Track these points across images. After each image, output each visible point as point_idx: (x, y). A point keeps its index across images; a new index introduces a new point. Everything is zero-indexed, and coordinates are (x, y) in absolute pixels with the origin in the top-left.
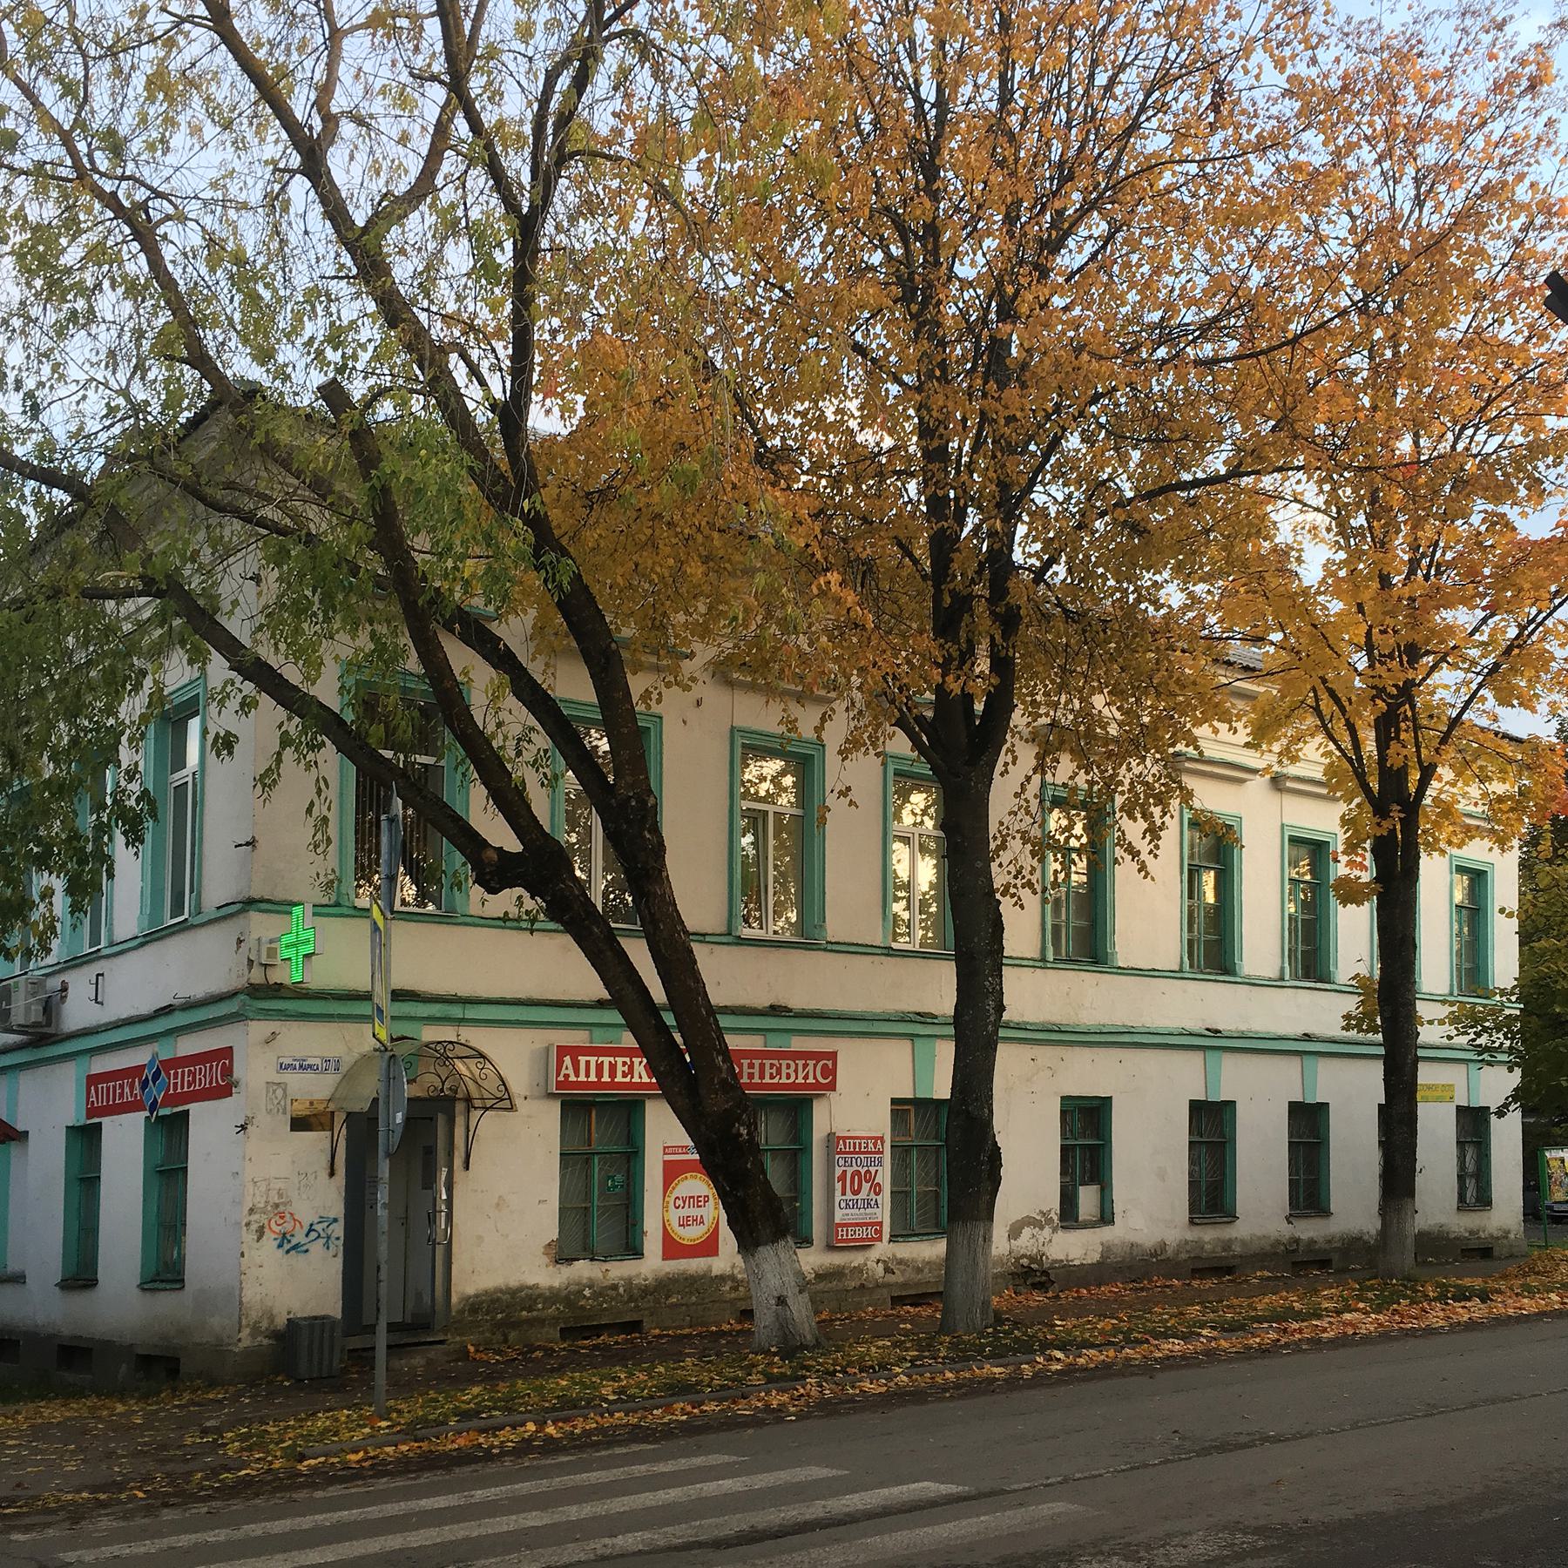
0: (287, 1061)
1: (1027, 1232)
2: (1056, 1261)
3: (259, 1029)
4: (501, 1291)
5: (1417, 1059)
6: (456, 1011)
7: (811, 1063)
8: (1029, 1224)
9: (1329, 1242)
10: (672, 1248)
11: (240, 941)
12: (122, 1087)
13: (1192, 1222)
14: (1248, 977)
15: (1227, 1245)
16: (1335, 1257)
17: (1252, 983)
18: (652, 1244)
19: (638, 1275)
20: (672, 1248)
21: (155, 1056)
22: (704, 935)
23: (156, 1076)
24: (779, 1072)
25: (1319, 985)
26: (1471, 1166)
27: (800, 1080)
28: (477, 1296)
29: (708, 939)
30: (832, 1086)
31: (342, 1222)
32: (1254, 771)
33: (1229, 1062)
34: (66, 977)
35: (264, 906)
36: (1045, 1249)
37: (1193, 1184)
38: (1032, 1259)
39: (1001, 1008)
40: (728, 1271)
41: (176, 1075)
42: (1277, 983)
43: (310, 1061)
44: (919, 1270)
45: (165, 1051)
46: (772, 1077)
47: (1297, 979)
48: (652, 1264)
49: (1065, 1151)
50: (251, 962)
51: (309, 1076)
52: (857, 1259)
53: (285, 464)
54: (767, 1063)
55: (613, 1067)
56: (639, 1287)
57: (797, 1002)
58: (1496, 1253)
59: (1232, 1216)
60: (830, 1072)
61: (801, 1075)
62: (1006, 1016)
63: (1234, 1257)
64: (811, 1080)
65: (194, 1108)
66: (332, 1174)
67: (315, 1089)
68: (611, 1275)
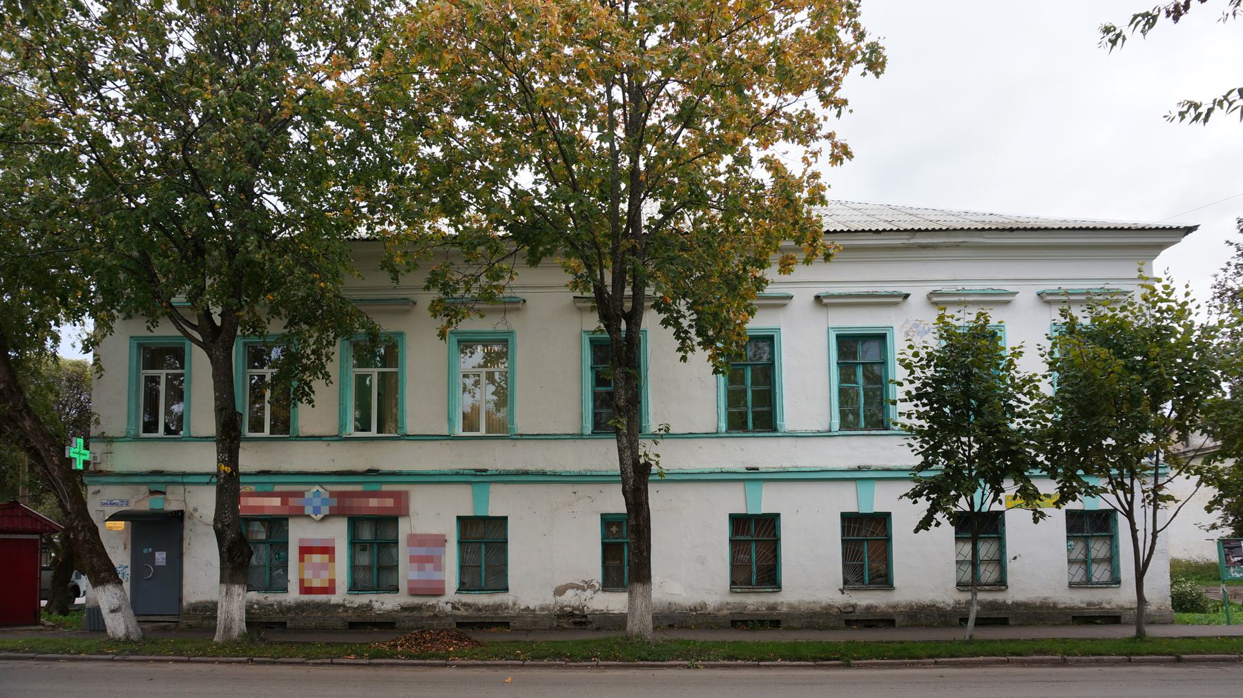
0: (105, 501)
2: (594, 610)
4: (208, 602)
9: (894, 607)
10: (306, 590)
15: (773, 608)
16: (898, 620)
18: (293, 586)
19: (285, 601)
20: (306, 590)
25: (853, 433)
28: (196, 603)
29: (324, 439)
31: (129, 568)
36: (587, 603)
38: (577, 609)
40: (341, 602)
43: (115, 501)
44: (479, 610)
48: (293, 595)
52: (432, 601)
53: (541, 630)
56: (285, 606)
57: (385, 467)
58: (1122, 621)
62: (620, 486)
63: (780, 614)
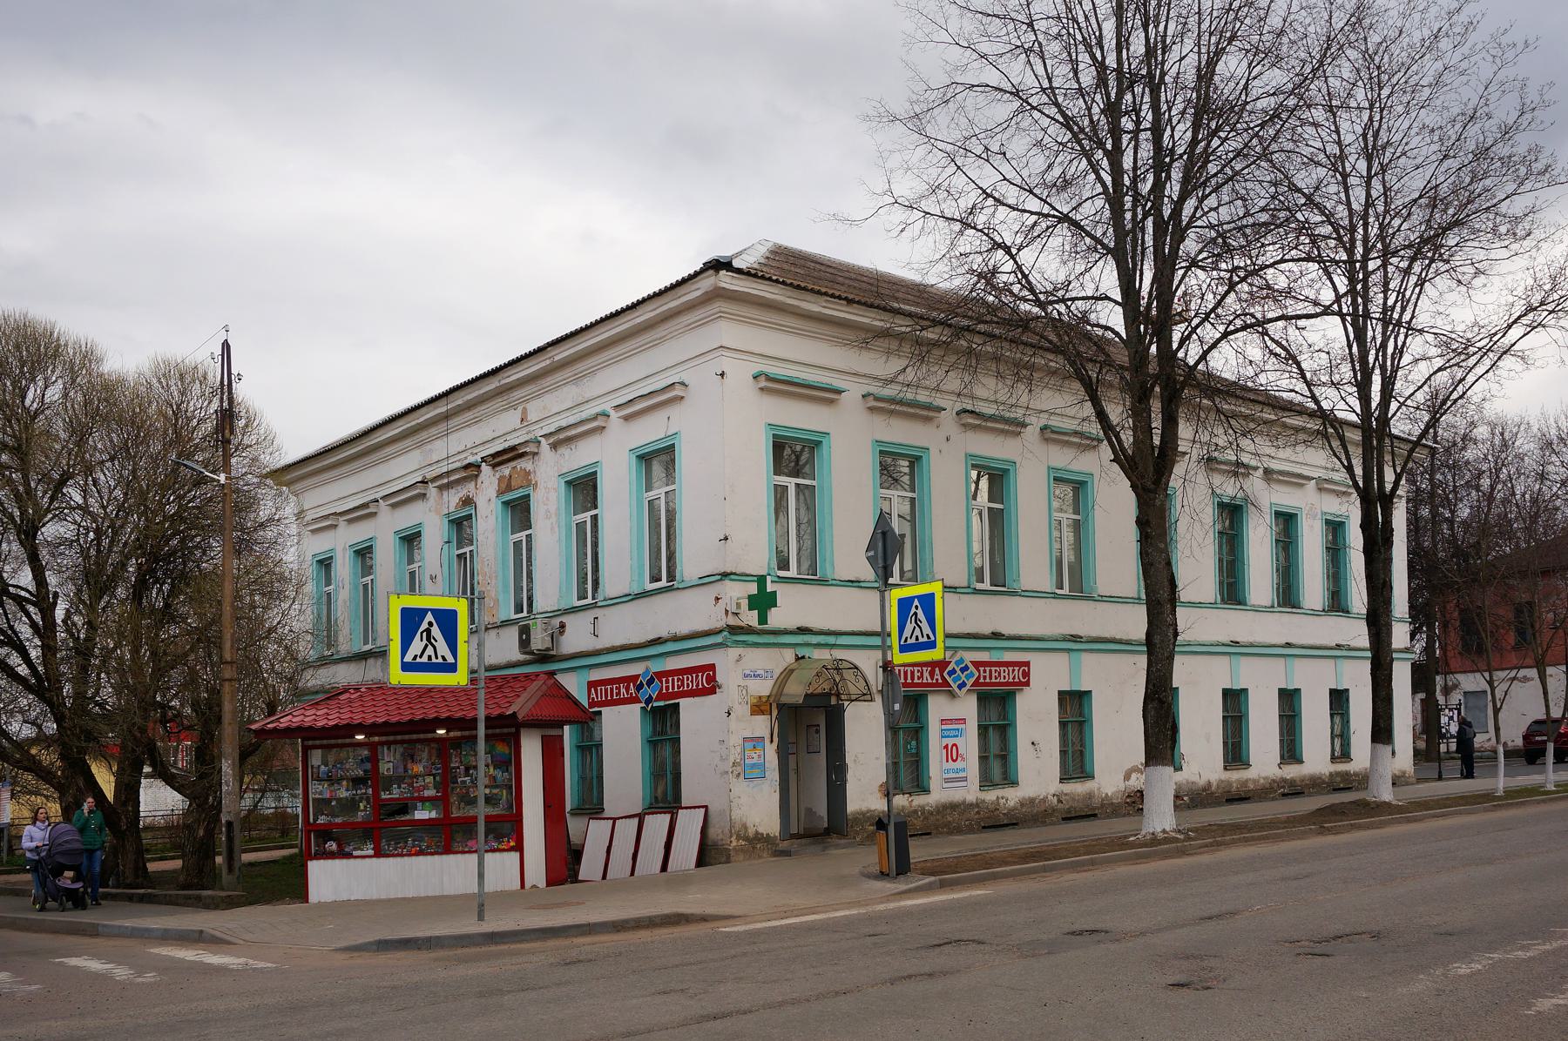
0: (747, 672)
1: (1134, 776)
3: (734, 652)
5: (1392, 660)
6: (831, 640)
7: (1016, 669)
8: (1135, 771)
11: (717, 599)
12: (618, 688)
13: (1225, 768)
14: (1254, 606)
15: (1245, 783)
17: (1256, 610)
19: (928, 804)
21: (647, 670)
22: (956, 588)
23: (650, 682)
24: (1000, 675)
25: (1294, 610)
26: (1337, 730)
27: (1011, 680)
29: (958, 590)
30: (1027, 684)
32: (1309, 478)
33: (1299, 664)
34: (564, 619)
35: (733, 577)
37: (1225, 744)
39: (1176, 634)
41: (667, 682)
42: (1269, 609)
45: (656, 666)
46: (919, 679)
47: (1279, 605)
49: (1224, 718)
50: (727, 611)
51: (758, 681)
54: (993, 669)
55: (912, 673)
59: (1300, 761)
60: (1026, 674)
61: (1011, 677)
64: (1016, 680)
65: (684, 703)
66: (772, 741)
67: (764, 688)
68: (914, 804)
